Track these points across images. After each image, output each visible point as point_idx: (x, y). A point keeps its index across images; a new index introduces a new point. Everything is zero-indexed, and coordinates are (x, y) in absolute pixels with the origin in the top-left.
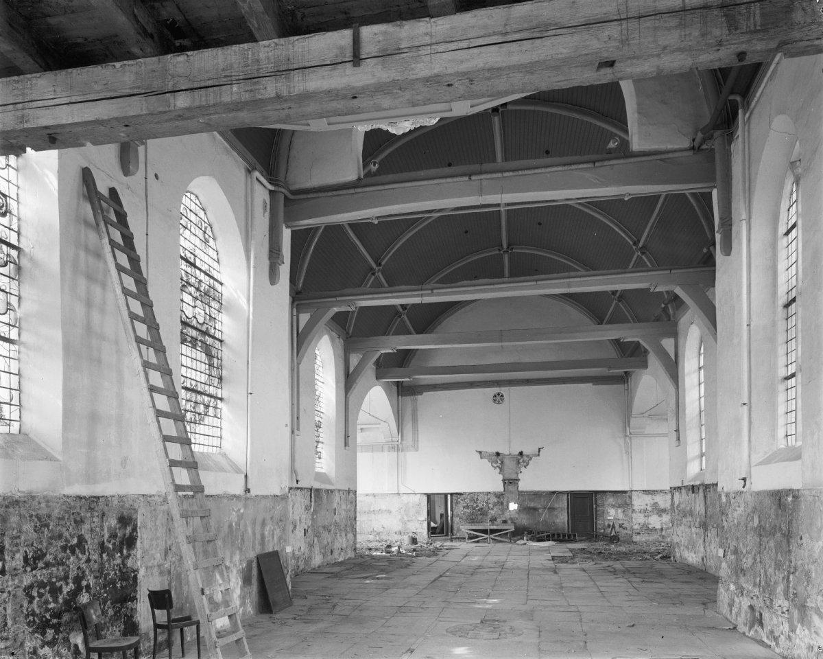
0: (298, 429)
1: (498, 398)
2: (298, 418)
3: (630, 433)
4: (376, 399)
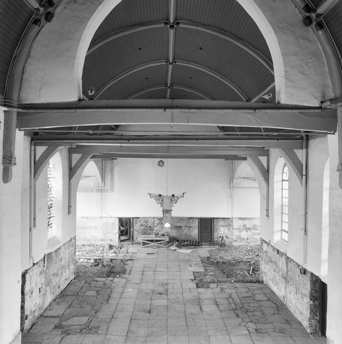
0: (35, 226)
1: (161, 163)
2: (34, 219)
3: (233, 187)
4: (91, 168)
